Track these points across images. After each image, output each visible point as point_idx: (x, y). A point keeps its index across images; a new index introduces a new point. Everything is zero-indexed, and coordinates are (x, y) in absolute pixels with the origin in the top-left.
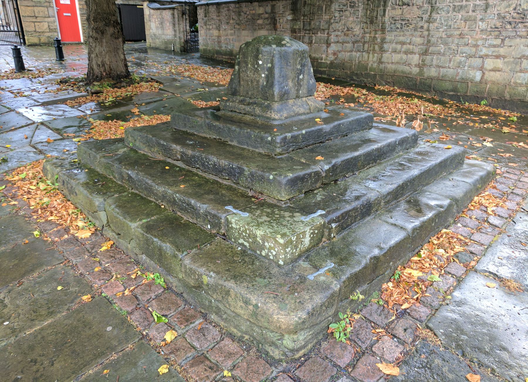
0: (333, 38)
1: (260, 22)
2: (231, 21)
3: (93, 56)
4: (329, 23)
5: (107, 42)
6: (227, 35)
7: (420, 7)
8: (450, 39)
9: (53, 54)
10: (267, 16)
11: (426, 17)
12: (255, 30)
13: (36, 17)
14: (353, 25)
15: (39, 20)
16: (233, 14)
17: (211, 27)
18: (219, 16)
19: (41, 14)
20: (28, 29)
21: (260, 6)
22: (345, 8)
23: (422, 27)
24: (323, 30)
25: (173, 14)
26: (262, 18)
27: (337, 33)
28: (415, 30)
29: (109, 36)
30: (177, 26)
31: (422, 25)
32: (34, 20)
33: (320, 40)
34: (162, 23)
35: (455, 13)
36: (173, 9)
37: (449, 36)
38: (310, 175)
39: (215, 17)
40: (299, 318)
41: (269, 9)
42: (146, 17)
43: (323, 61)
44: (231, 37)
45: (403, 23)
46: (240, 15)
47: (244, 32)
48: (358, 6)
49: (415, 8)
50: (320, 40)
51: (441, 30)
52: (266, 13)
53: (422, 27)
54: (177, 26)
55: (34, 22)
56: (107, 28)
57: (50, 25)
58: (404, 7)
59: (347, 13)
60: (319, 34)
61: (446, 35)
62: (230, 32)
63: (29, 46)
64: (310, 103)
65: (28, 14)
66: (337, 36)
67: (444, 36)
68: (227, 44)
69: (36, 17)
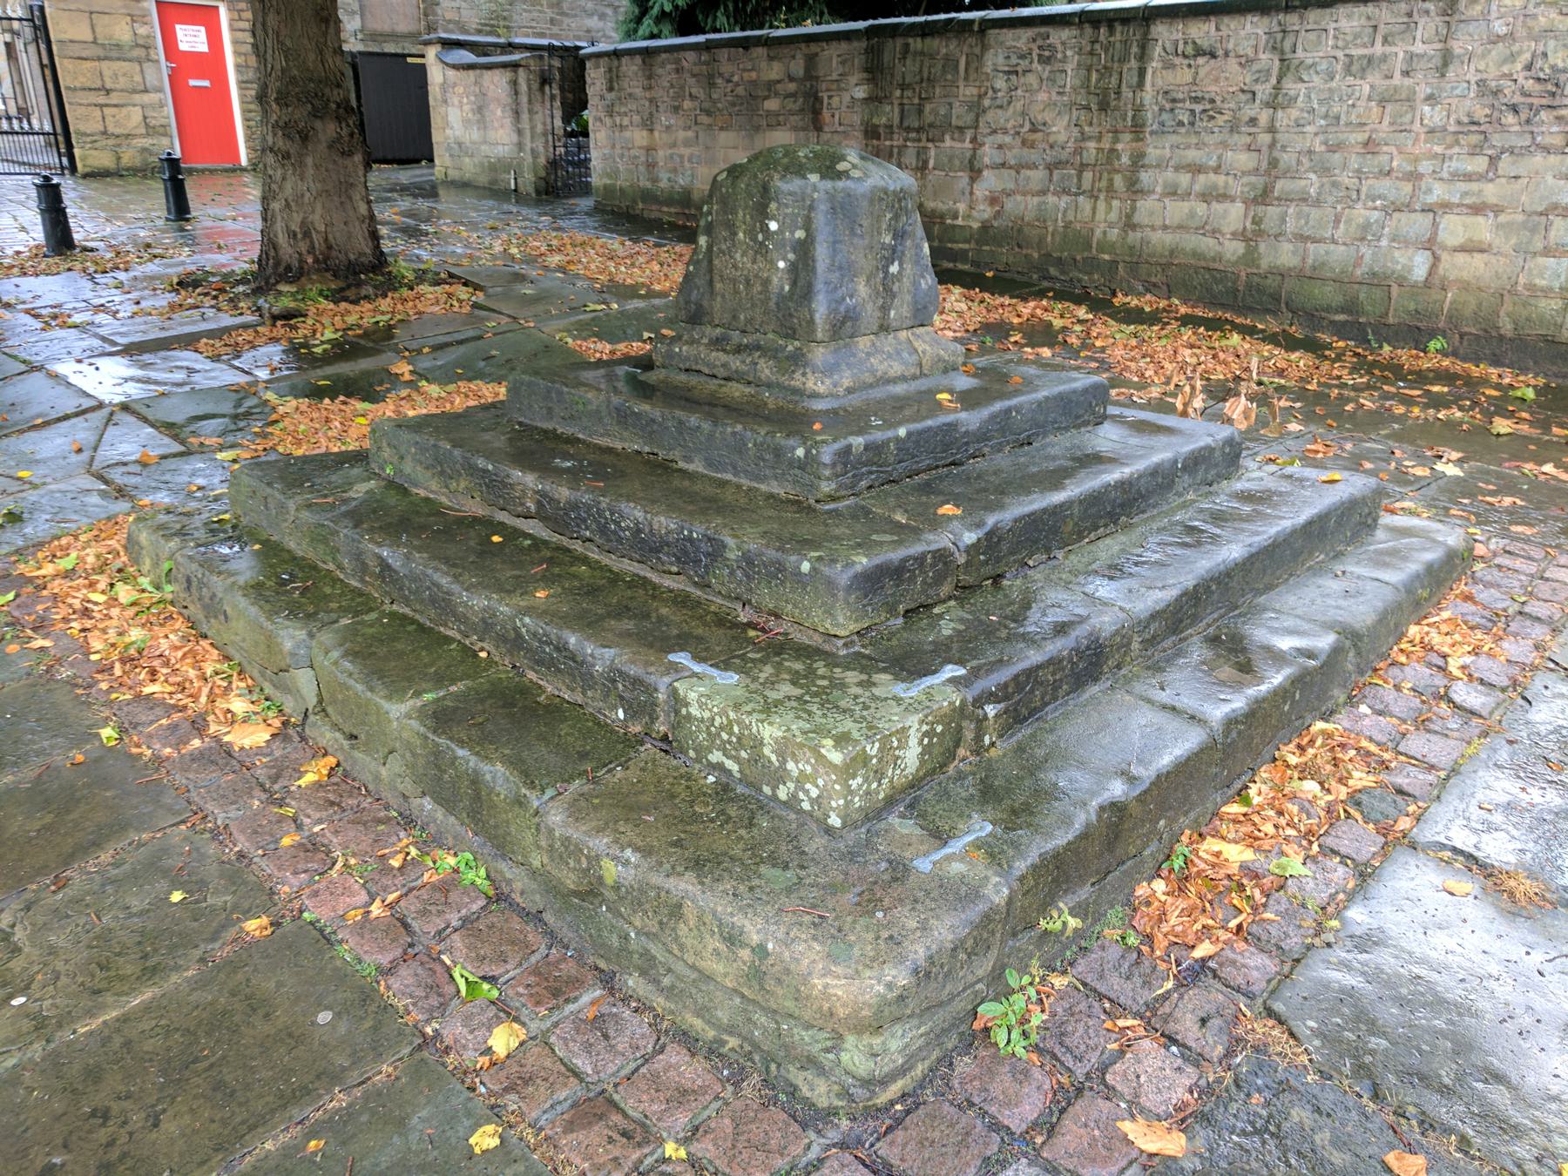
0: (988, 154)
2: (687, 104)
3: (276, 206)
4: (977, 108)
5: (316, 167)
6: (674, 145)
7: (1246, 62)
9: (156, 199)
11: (1264, 90)
12: (757, 129)
13: (108, 92)
15: (114, 98)
16: (691, 81)
17: (626, 121)
18: (650, 88)
20: (82, 128)
21: (771, 58)
22: (1024, 64)
24: (961, 129)
26: (777, 94)
27: (1000, 138)
29: (322, 147)
30: (525, 116)
31: (1252, 113)
33: (951, 159)
36: (514, 66)
37: (1332, 149)
38: (920, 559)
39: (638, 92)
40: (889, 986)
41: (797, 67)
43: (960, 222)
45: (1198, 108)
46: (712, 85)
48: (1065, 60)
49: (1232, 63)
50: (951, 159)
51: (1308, 129)
53: (1253, 121)
54: (525, 116)
55: (102, 106)
56: (318, 124)
57: (150, 113)
58: (1201, 60)
60: (948, 142)
64: (920, 346)
65: (82, 81)
68: (675, 170)
69: (108, 92)
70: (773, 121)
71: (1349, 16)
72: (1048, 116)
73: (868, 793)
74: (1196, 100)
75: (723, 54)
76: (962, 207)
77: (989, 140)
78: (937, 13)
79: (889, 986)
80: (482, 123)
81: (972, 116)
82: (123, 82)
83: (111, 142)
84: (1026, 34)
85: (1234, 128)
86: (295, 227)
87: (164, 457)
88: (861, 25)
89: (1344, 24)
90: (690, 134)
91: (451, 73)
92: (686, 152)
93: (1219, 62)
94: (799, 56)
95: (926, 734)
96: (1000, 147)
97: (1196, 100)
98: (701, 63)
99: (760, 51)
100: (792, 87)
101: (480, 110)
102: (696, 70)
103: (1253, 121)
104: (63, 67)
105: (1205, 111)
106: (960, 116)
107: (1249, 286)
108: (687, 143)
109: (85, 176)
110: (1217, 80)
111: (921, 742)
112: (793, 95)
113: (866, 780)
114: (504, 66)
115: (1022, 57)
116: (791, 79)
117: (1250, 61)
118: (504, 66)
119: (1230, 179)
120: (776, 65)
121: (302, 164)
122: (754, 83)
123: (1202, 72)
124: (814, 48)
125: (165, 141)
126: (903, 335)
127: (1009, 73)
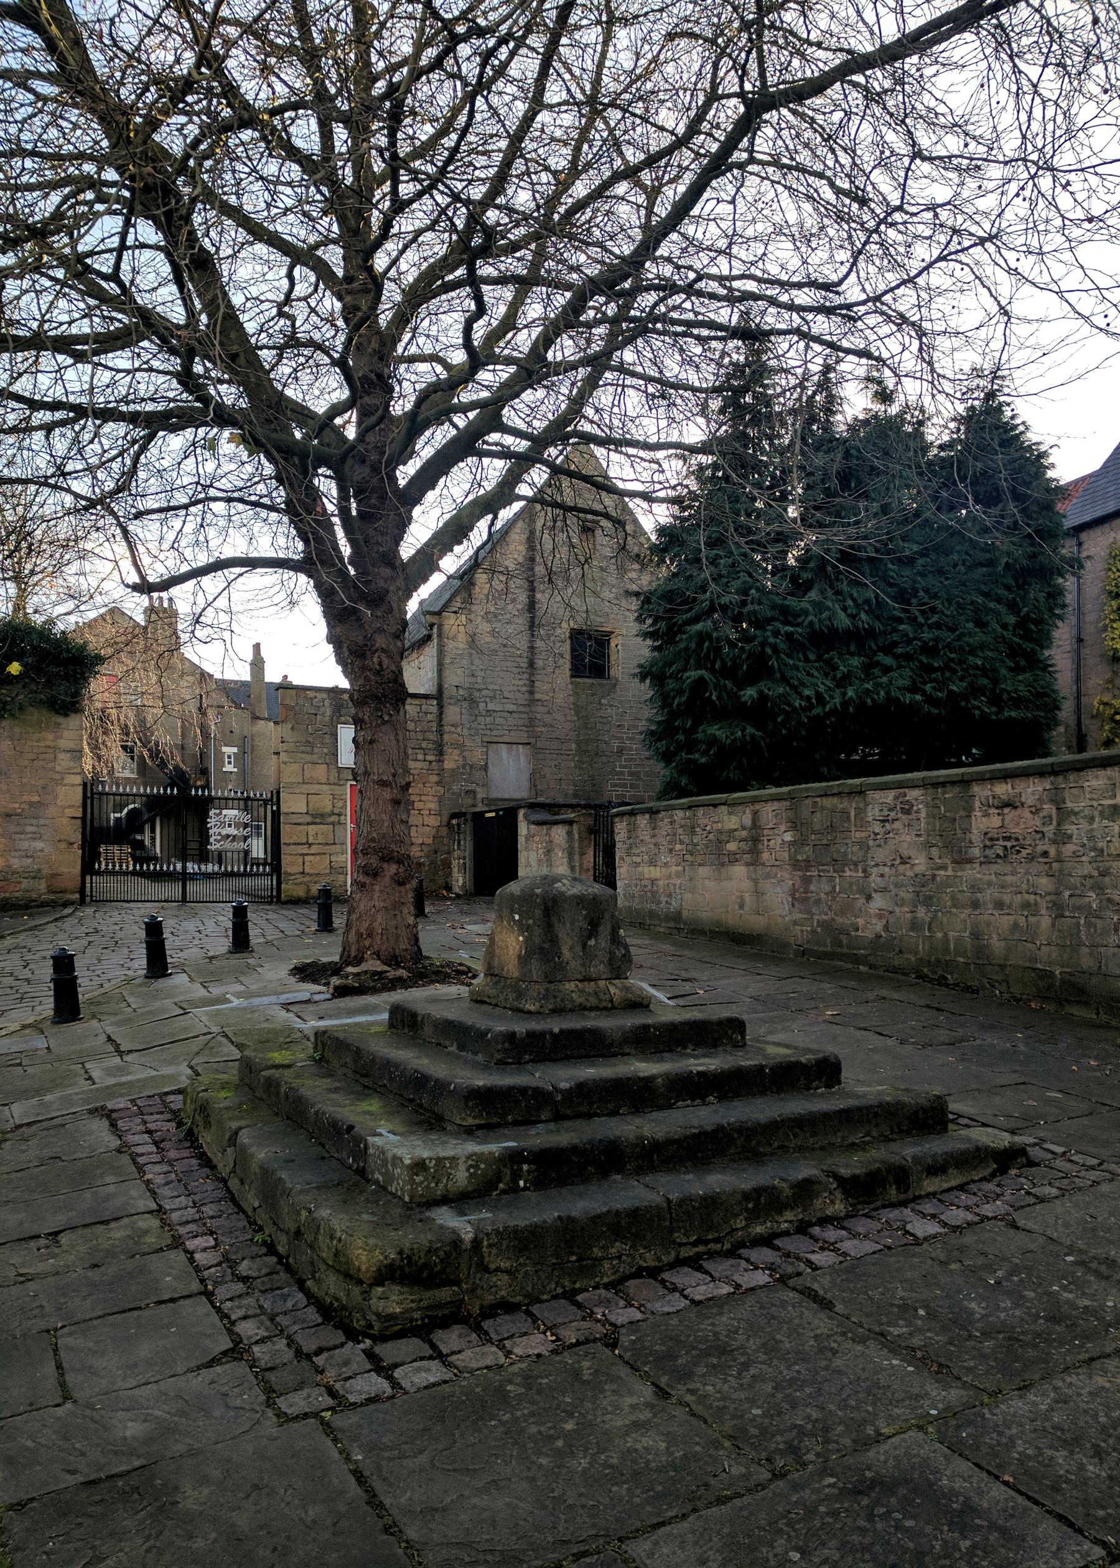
0: (875, 881)
1: (732, 846)
2: (678, 847)
3: (354, 917)
4: (863, 845)
5: (381, 891)
6: (670, 877)
7: (1036, 811)
8: (1107, 879)
9: (311, 914)
10: (744, 833)
11: (1050, 830)
12: (723, 865)
13: (310, 845)
14: (912, 853)
15: (314, 849)
16: (680, 831)
17: (639, 860)
18: (654, 836)
19: (320, 839)
20: (289, 870)
21: (730, 814)
22: (893, 814)
23: (1045, 854)
24: (856, 864)
25: (569, 833)
26: (735, 839)
27: (882, 869)
28: (1031, 858)
29: (387, 879)
30: (577, 857)
31: (1045, 848)
32: (304, 850)
33: (851, 885)
34: (549, 852)
35: (1106, 822)
36: (570, 823)
37: (1103, 874)
38: (523, 1090)
39: (647, 838)
40: (386, 1257)
41: (747, 820)
42: (521, 840)
43: (860, 933)
44: (678, 882)
45: (1009, 844)
46: (693, 833)
47: (701, 869)
48: (918, 812)
49: (1026, 813)
50: (851, 885)
51: (1084, 859)
52: (744, 828)
53: (1045, 854)
54: (577, 857)
55: (304, 855)
56: (385, 865)
57: (333, 858)
58: (1006, 810)
59: (897, 825)
60: (848, 873)
61: (1097, 869)
62: (674, 869)
63: (286, 903)
64: (613, 990)
65: (295, 839)
66: (882, 876)
67: (1095, 873)
68: (670, 896)
69: (310, 845)
71: (1097, 777)
73: (428, 1187)
75: (700, 812)
77: (874, 871)
78: (993, 763)
80: (550, 864)
87: (459, 1352)
88: (785, 789)
89: (1094, 783)
91: (532, 827)
99: (723, 809)
104: (285, 829)
105: (1013, 847)
110: (1018, 824)
111: (468, 1170)
117: (1038, 811)
121: (373, 890)
122: (720, 831)
123: (1008, 818)
124: (757, 807)
127: (882, 821)
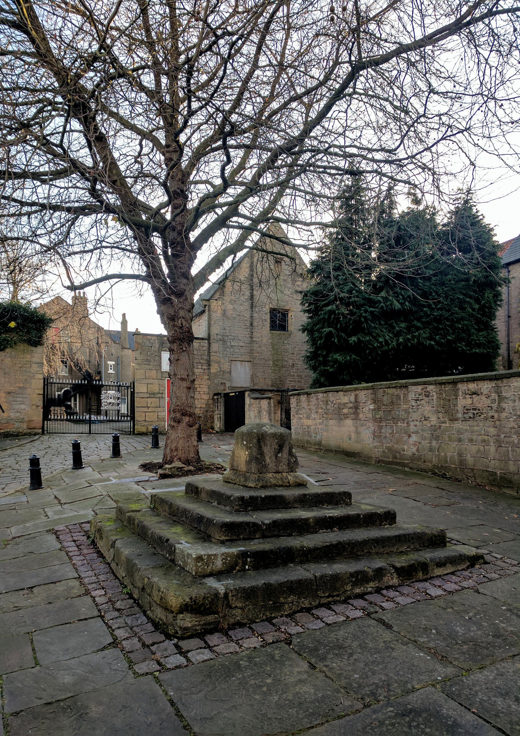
2: (320, 411)
3: (169, 441)
7: (488, 397)
9: (149, 440)
11: (495, 406)
12: (341, 419)
15: (150, 410)
16: (321, 403)
17: (302, 416)
18: (309, 405)
20: (139, 419)
21: (344, 395)
22: (421, 397)
29: (184, 424)
30: (273, 415)
31: (493, 414)
39: (305, 406)
40: (184, 601)
41: (353, 399)
43: (405, 453)
45: (475, 412)
46: (327, 404)
48: (432, 396)
49: (484, 398)
51: (510, 419)
53: (493, 417)
54: (273, 415)
56: (183, 418)
58: (474, 396)
60: (400, 424)
70: (345, 416)
72: (430, 415)
73: (203, 568)
74: (475, 409)
75: (330, 394)
76: (406, 447)
77: (412, 423)
79: (184, 601)
81: (406, 415)
82: (153, 405)
83: (146, 424)
84: (420, 387)
85: (486, 419)
86: (173, 448)
90: (321, 421)
91: (252, 400)
92: (320, 427)
93: (480, 397)
94: (353, 394)
95: (224, 559)
96: (416, 426)
97: (475, 409)
98: (323, 397)
100: (351, 405)
101: (259, 412)
102: (322, 399)
103: (493, 417)
106: (403, 414)
107: (501, 478)
108: (320, 424)
109: (137, 434)
111: (222, 560)
112: (351, 408)
113: (203, 564)
114: (267, 398)
115: (419, 395)
116: (351, 403)
118: (267, 398)
119: (489, 437)
120: (346, 398)
123: (475, 400)
124: (357, 392)
125: (163, 423)
126: (284, 474)
